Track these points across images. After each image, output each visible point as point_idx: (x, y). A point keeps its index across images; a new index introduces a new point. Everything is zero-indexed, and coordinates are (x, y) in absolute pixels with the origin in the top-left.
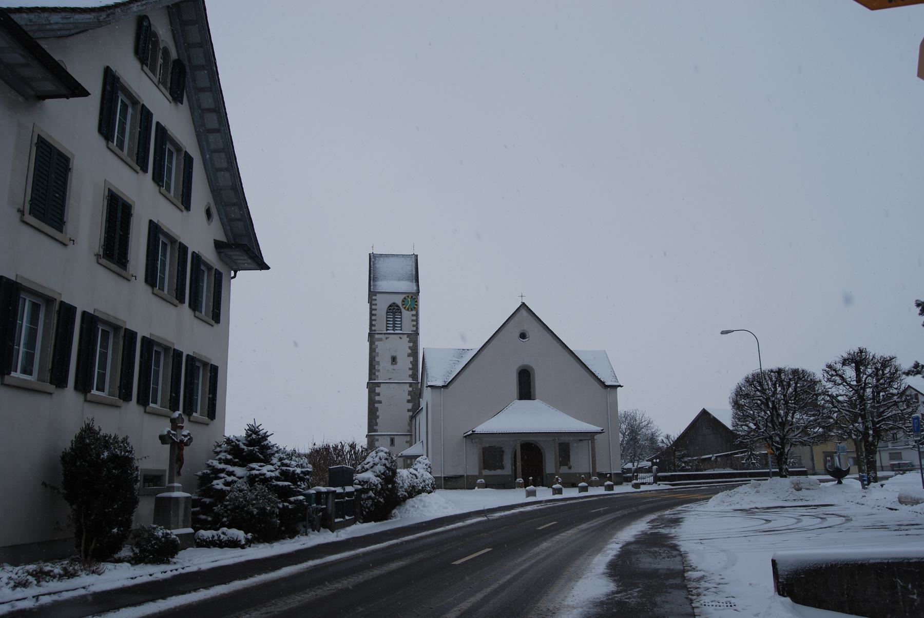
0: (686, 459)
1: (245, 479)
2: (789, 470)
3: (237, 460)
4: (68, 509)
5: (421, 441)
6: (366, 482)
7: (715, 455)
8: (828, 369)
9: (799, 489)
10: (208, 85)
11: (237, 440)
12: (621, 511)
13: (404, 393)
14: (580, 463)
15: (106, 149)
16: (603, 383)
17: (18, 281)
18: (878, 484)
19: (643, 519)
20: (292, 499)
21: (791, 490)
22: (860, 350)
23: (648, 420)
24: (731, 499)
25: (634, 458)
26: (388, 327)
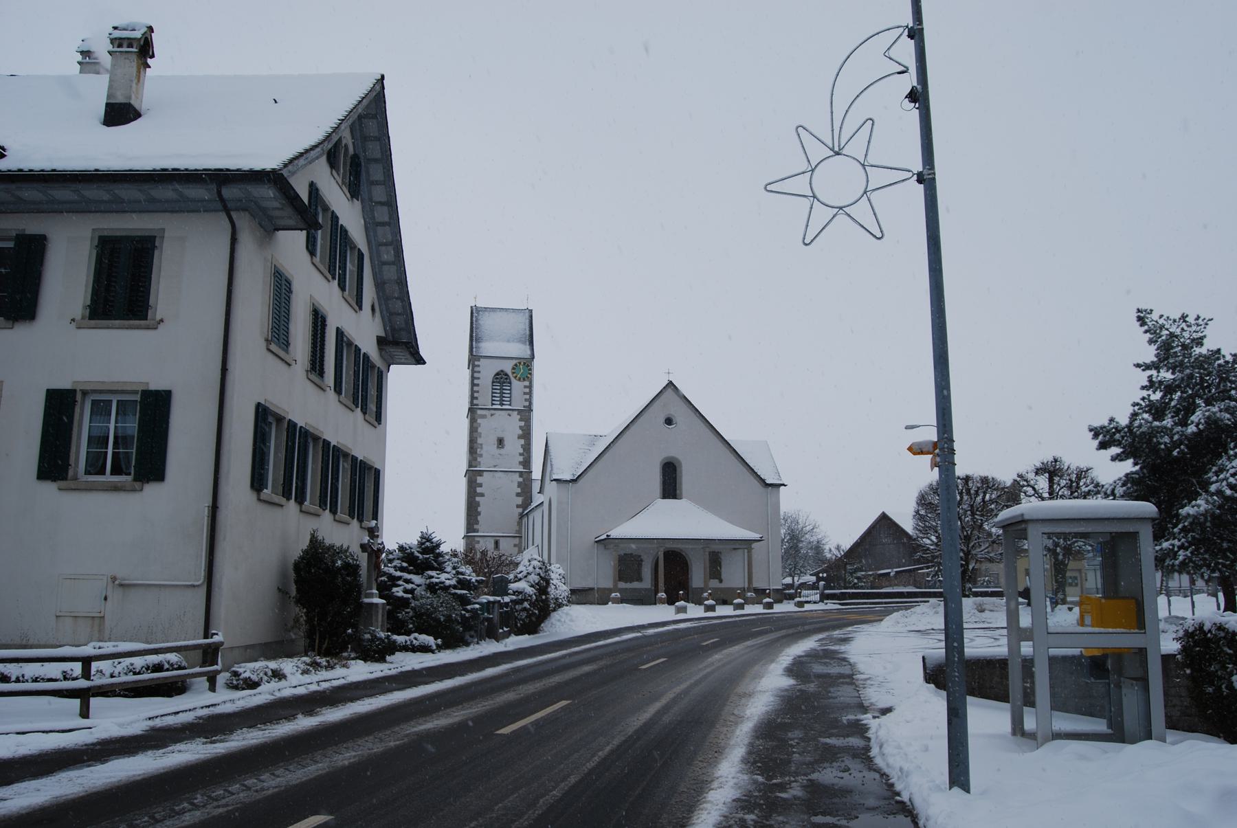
0: (860, 574)
1: (423, 587)
2: (973, 590)
3: (411, 568)
4: (299, 611)
5: (535, 545)
6: (521, 593)
7: (895, 570)
8: (1018, 479)
9: (982, 611)
10: (382, 179)
11: (410, 547)
12: (785, 631)
13: (511, 485)
14: (733, 576)
15: (310, 264)
16: (763, 481)
17: (266, 405)
18: (1065, 607)
19: (811, 638)
20: (469, 607)
21: (973, 611)
22: (1054, 459)
23: (813, 524)
24: (907, 620)
25: (794, 571)
26: (494, 400)
